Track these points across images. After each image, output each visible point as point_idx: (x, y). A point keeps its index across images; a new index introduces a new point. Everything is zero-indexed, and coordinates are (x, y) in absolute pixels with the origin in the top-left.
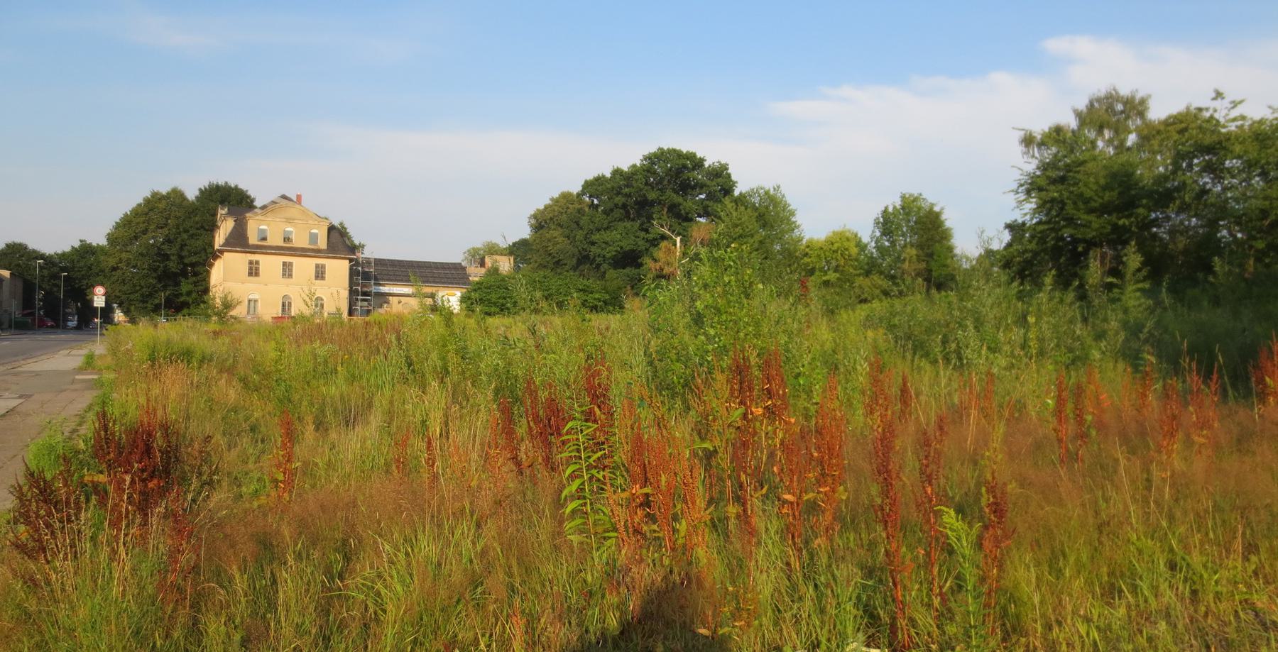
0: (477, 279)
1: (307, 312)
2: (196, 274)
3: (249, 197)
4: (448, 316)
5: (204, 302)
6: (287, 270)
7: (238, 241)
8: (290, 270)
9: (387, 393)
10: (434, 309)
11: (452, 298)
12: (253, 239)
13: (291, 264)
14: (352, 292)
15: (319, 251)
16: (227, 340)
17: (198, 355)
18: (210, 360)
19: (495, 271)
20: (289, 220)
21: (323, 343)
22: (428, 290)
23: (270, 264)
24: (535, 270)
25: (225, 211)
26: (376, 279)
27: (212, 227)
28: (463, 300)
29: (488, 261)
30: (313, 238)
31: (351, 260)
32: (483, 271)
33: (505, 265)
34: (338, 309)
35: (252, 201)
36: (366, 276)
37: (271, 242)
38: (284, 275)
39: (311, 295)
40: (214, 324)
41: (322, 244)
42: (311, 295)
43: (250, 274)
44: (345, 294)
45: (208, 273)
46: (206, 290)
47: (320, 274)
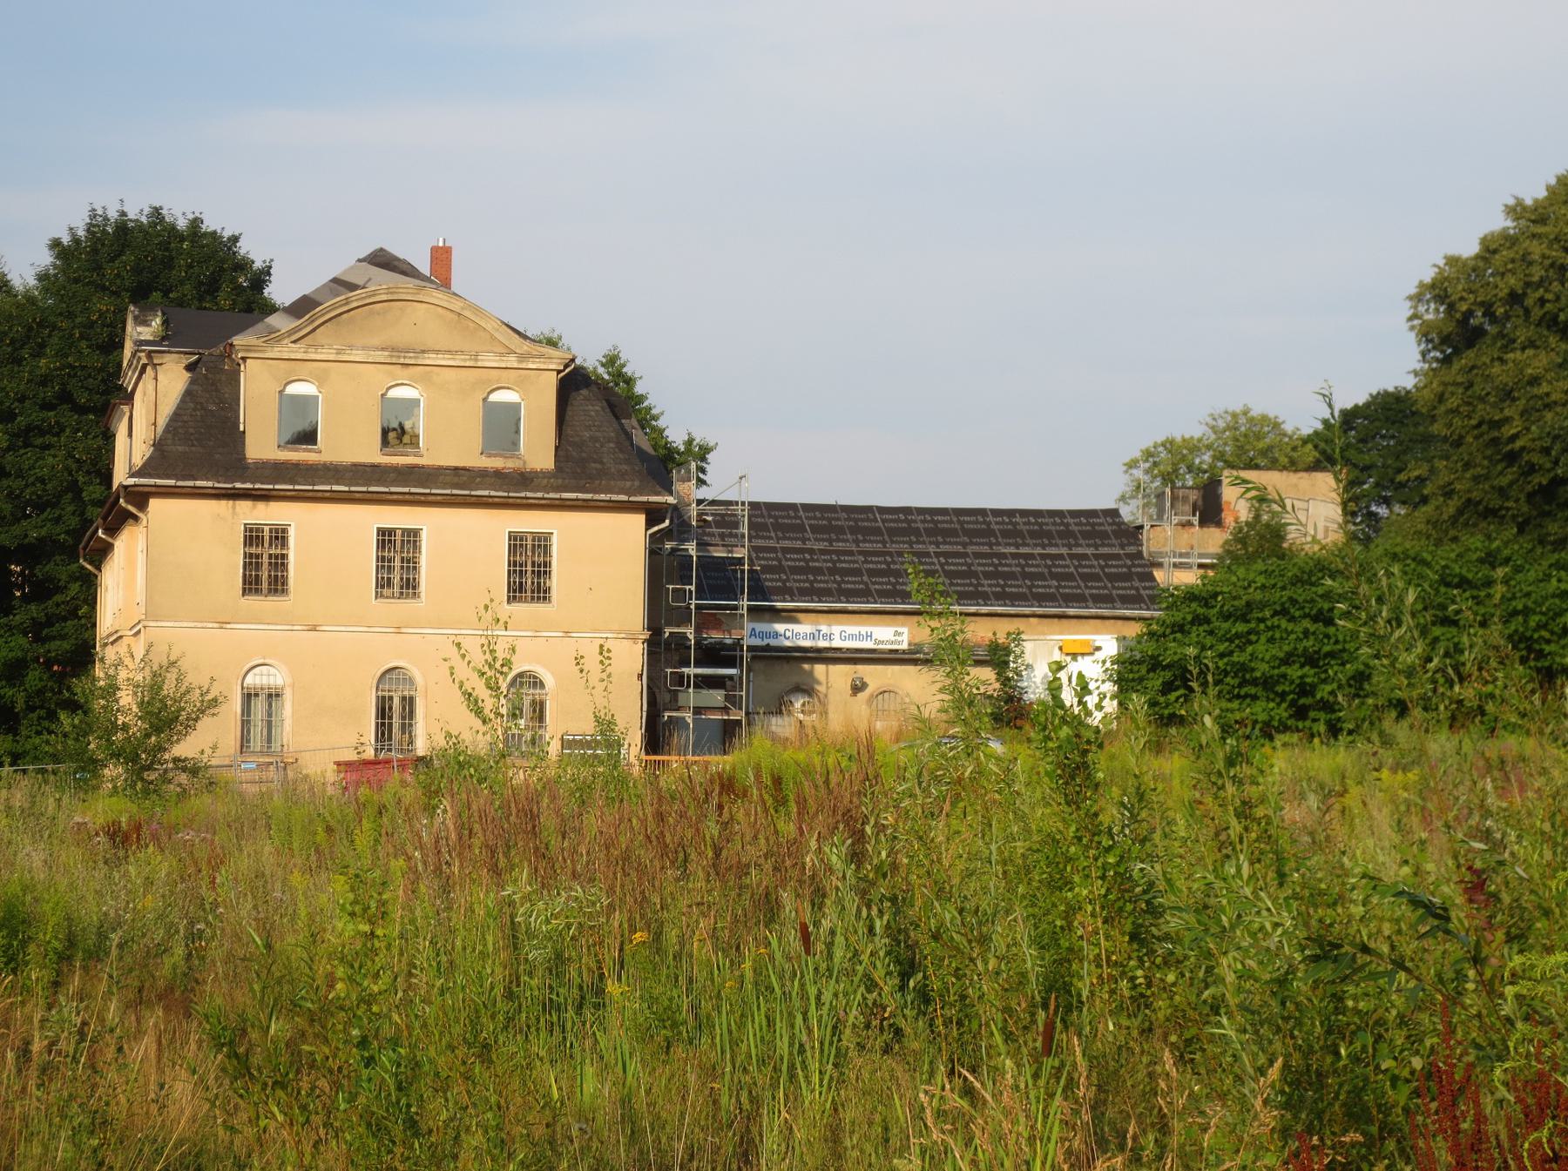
0: (1188, 578)
1: (476, 738)
2: (42, 590)
3: (243, 265)
4: (1075, 758)
5: (74, 706)
6: (397, 564)
7: (206, 451)
8: (411, 564)
9: (814, 1096)
10: (1010, 712)
11: (1074, 660)
12: (262, 441)
13: (412, 536)
14: (662, 650)
15: (524, 479)
16: (163, 867)
17: (49, 935)
18: (97, 954)
19: (1265, 539)
20: (403, 357)
21: (546, 882)
22: (981, 632)
23: (331, 540)
24: (1442, 531)
25: (152, 328)
26: (758, 591)
27: (110, 396)
28: (1128, 674)
29: (1237, 504)
30: (501, 426)
31: (653, 515)
32: (1213, 541)
33: (1315, 511)
34: (606, 725)
35: (260, 279)
36: (719, 579)
37: (335, 447)
38: (383, 584)
39: (495, 667)
40: (107, 805)
41: (537, 448)
42: (495, 667)
43: (251, 585)
44: (631, 657)
45: (89, 586)
46: (83, 655)
47: (529, 574)
